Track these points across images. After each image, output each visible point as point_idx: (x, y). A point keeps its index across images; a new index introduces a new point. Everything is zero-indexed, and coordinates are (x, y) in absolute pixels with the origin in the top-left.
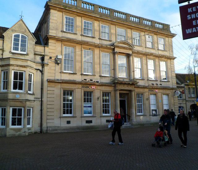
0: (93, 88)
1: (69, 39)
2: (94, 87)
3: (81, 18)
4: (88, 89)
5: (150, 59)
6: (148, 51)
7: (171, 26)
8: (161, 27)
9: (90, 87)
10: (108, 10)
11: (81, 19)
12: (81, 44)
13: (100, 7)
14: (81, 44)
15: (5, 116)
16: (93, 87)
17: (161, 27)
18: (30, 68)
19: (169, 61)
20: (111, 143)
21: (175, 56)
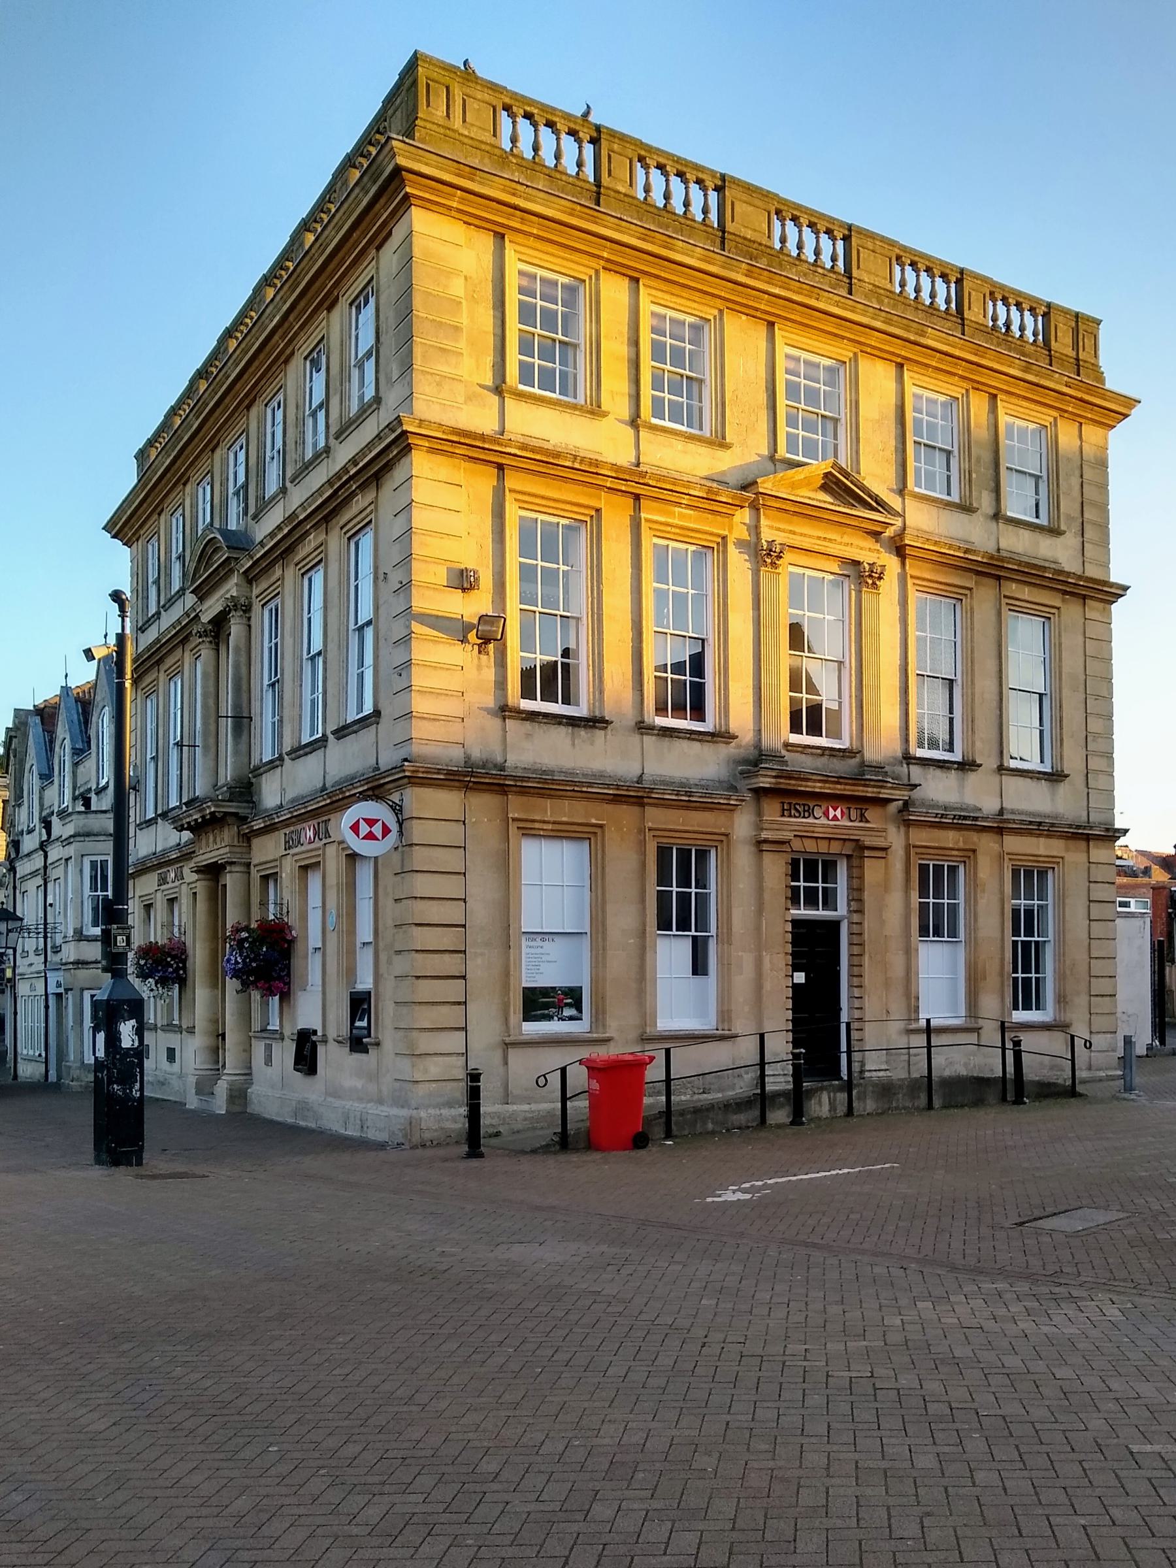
0: (835, 818)
1: (1028, 565)
2: (838, 813)
3: (486, 242)
4: (811, 820)
5: (1018, 607)
6: (1018, 543)
7: (1103, 332)
8: (1029, 334)
9: (818, 812)
10: (804, 221)
11: (763, 345)
12: (998, 578)
13: (644, 155)
14: (998, 578)
15: (1028, 932)
16: (832, 813)
17: (1029, 334)
18: (421, 689)
19: (1071, 612)
20: (213, 1273)
21: (1116, 576)
